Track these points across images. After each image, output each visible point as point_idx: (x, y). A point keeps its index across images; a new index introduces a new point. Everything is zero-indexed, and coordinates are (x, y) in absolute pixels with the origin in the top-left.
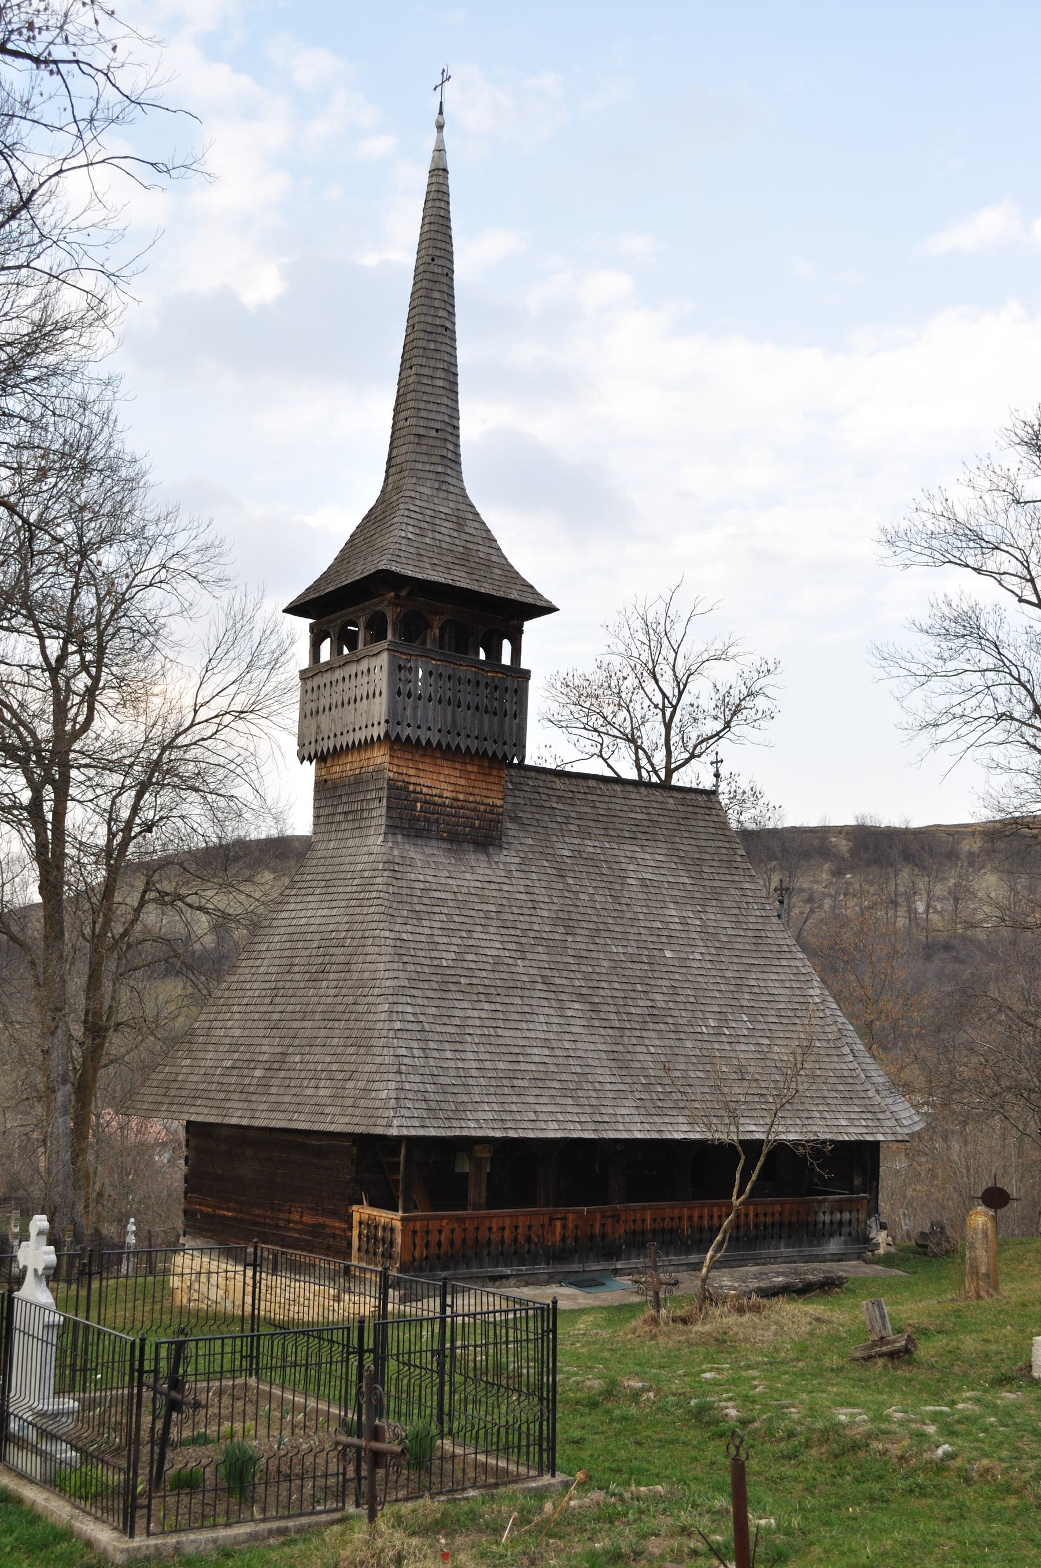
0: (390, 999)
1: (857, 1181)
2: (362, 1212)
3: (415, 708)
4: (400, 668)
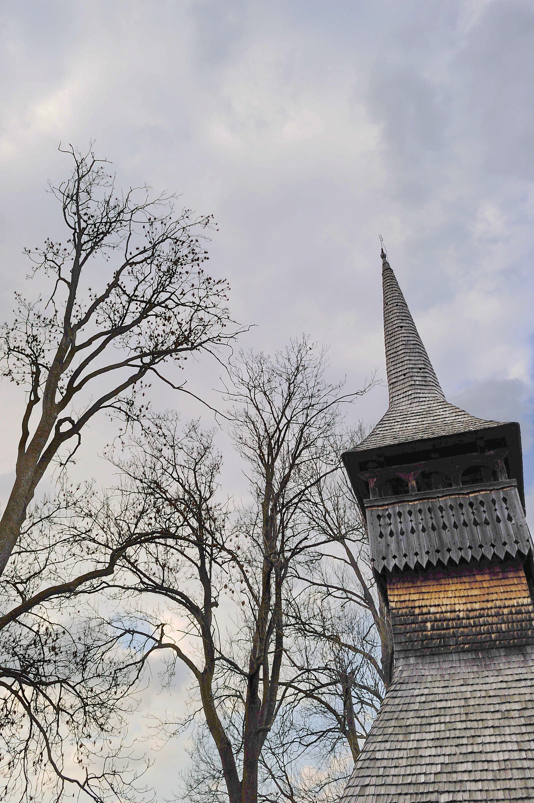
3: (398, 543)
4: (379, 517)
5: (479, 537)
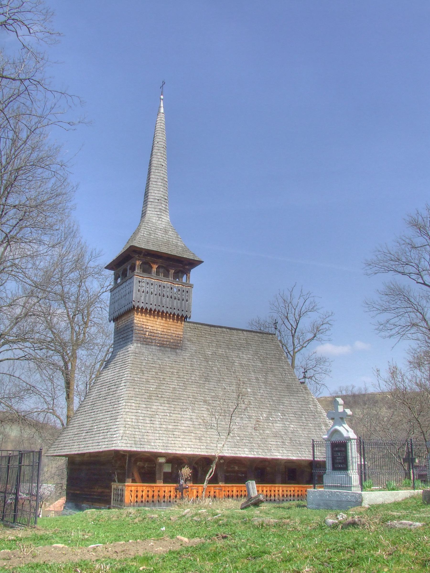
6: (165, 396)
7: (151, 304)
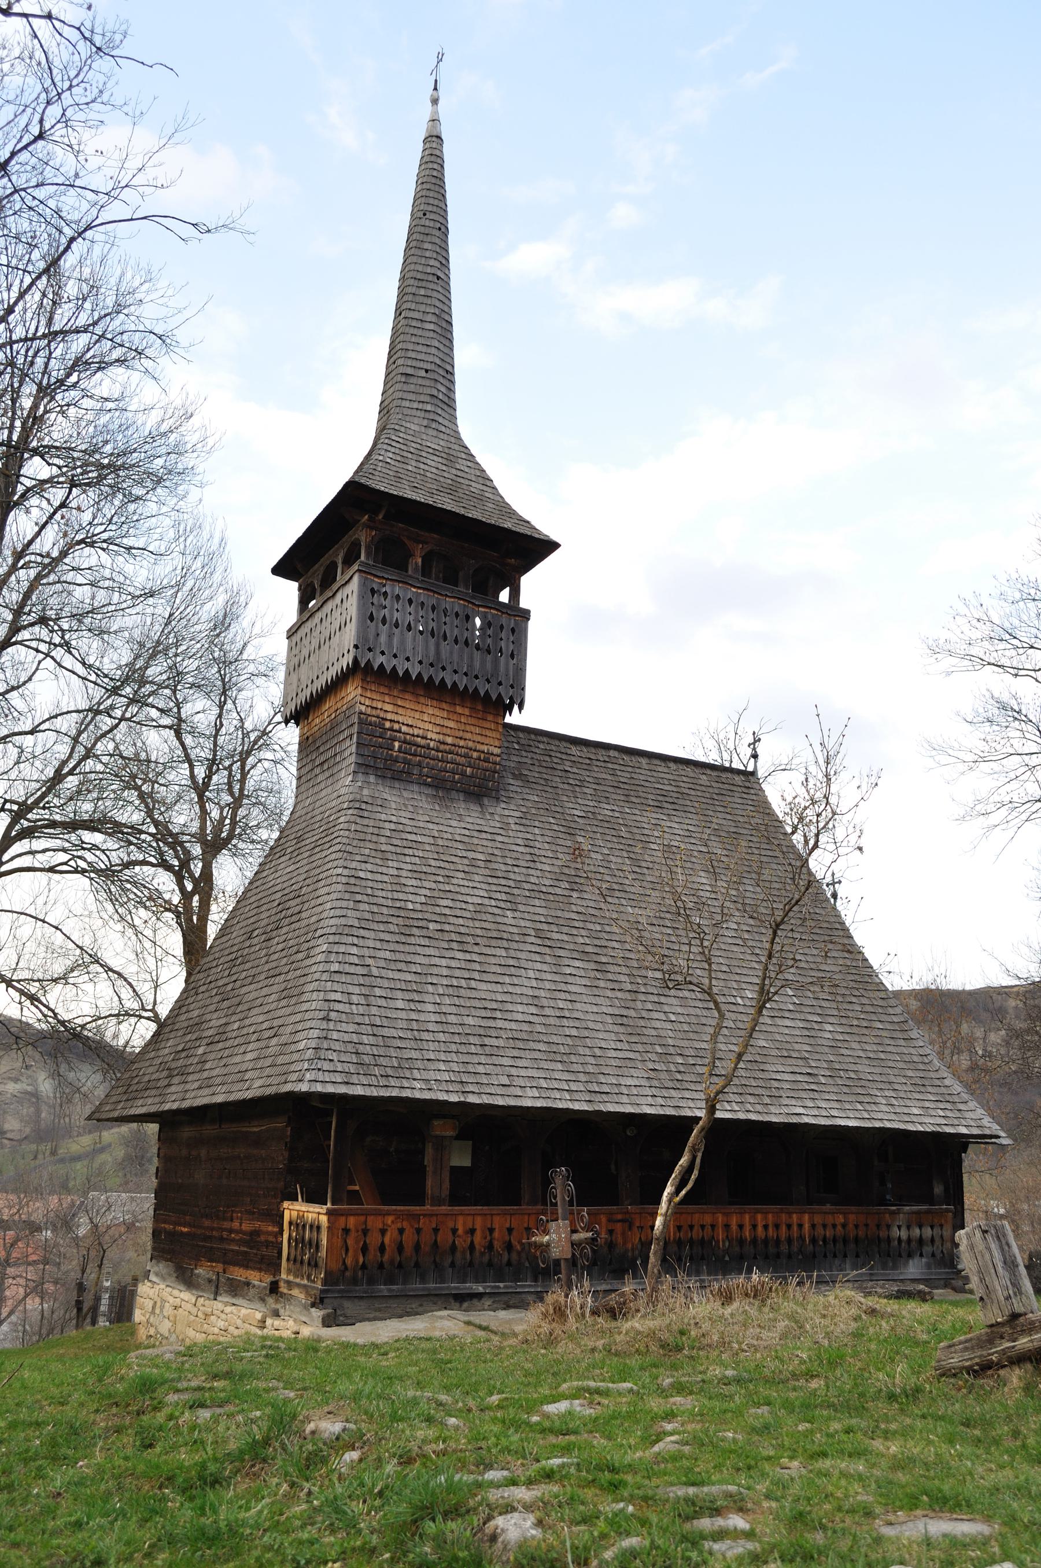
0: (331, 939)
1: (938, 1189)
2: (294, 1209)
3: (390, 636)
4: (373, 591)
5: (477, 664)
6: (452, 928)
7: (408, 659)
